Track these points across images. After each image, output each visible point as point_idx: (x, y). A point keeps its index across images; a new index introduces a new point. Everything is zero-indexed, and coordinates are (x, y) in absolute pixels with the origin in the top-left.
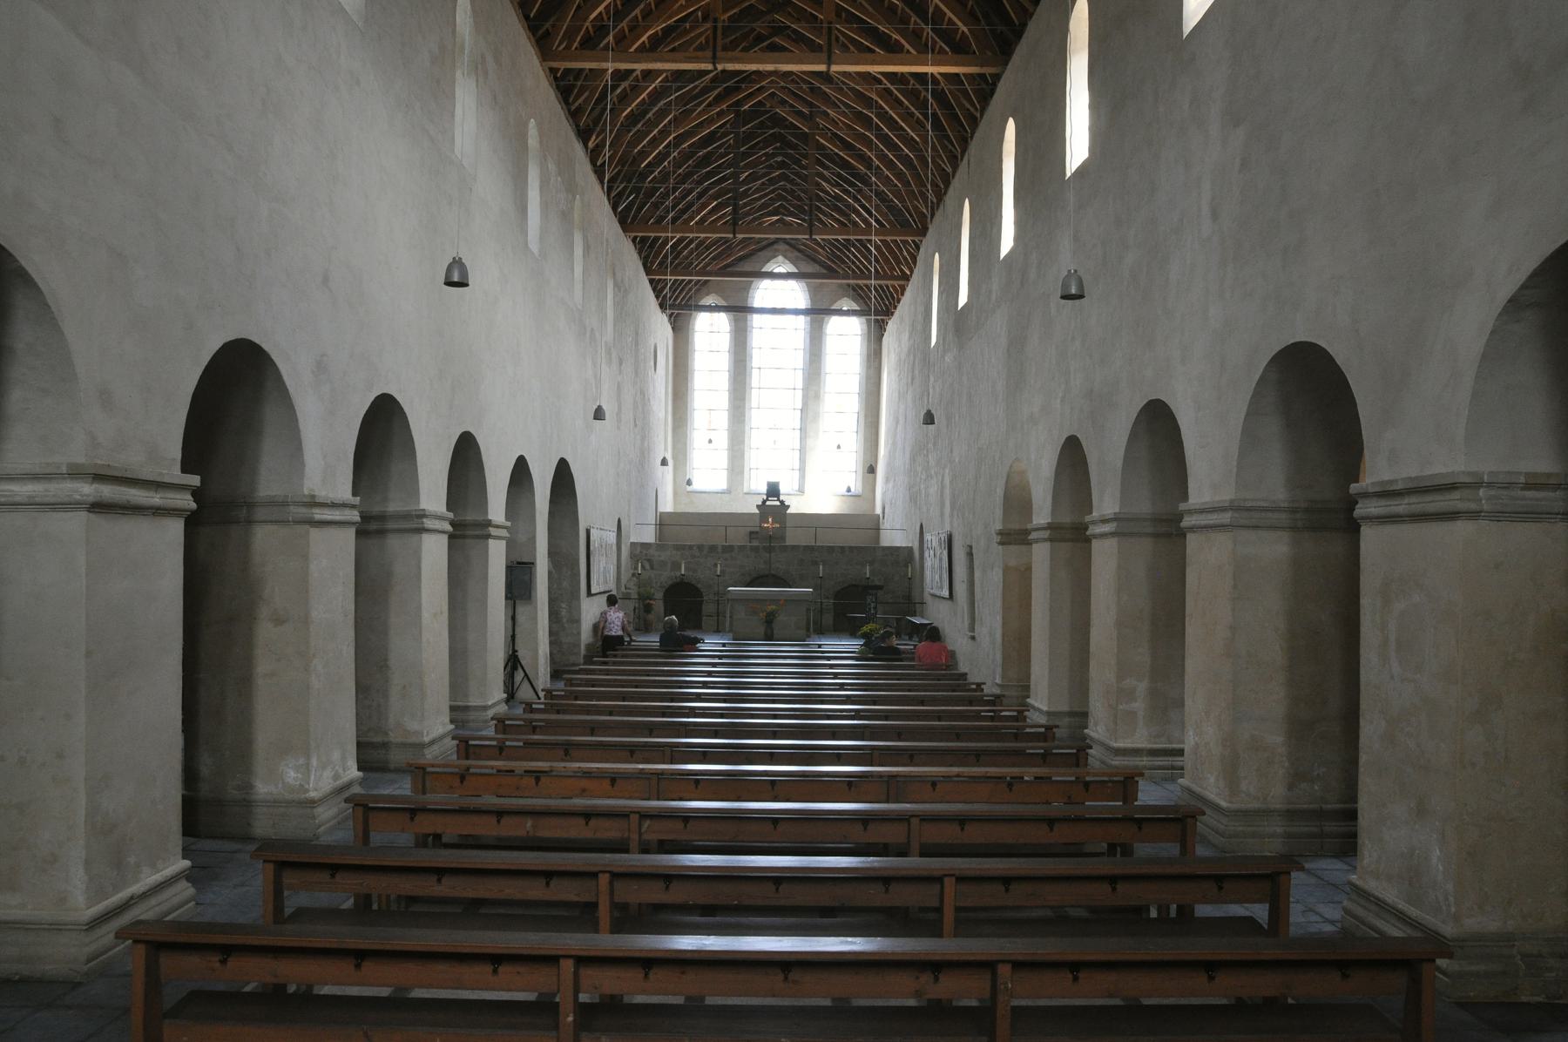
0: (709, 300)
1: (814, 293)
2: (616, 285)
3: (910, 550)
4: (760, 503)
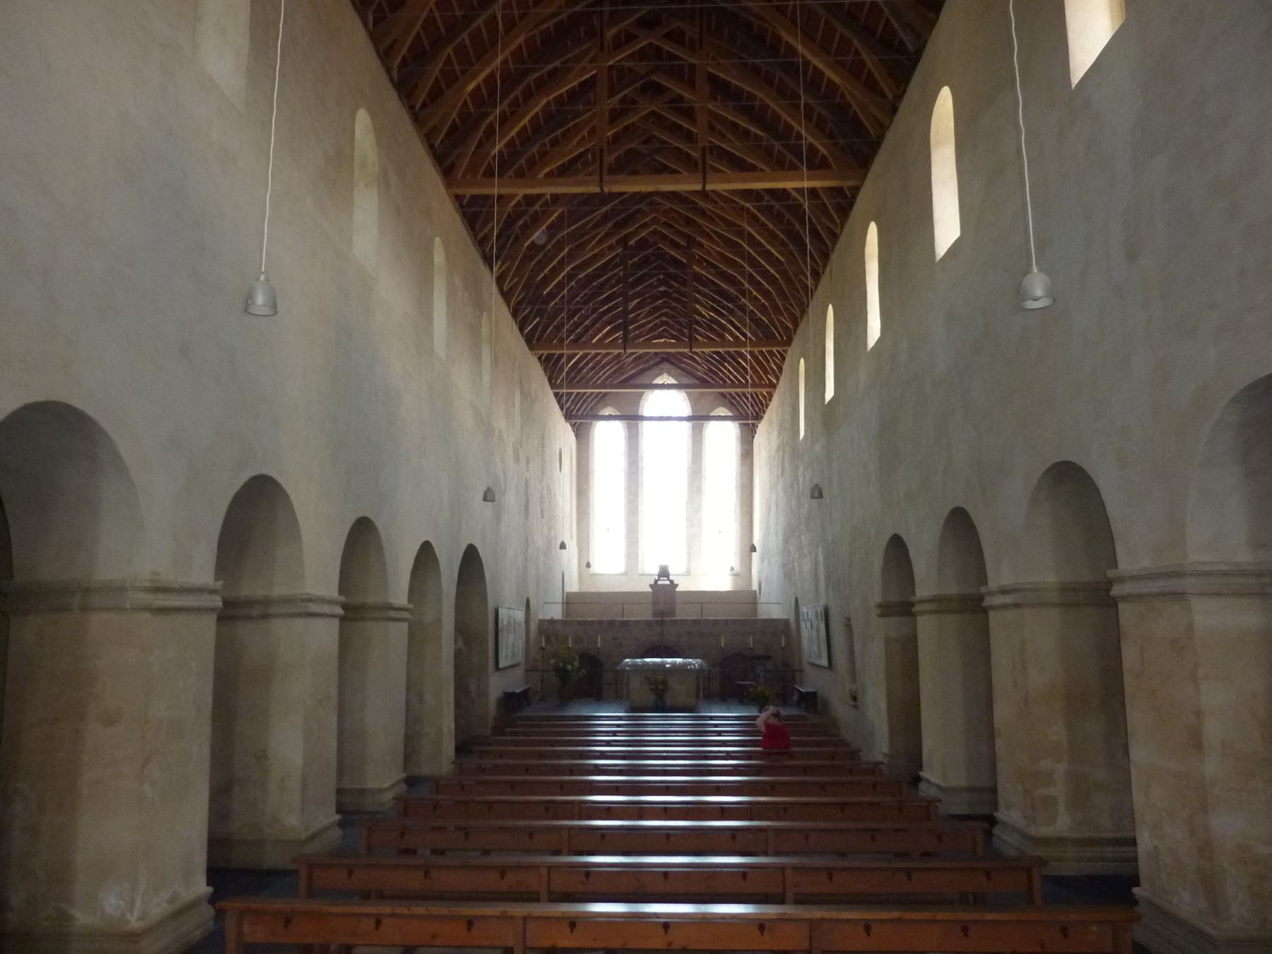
0: (607, 411)
1: (694, 402)
2: (522, 393)
3: (786, 622)
4: (653, 583)
